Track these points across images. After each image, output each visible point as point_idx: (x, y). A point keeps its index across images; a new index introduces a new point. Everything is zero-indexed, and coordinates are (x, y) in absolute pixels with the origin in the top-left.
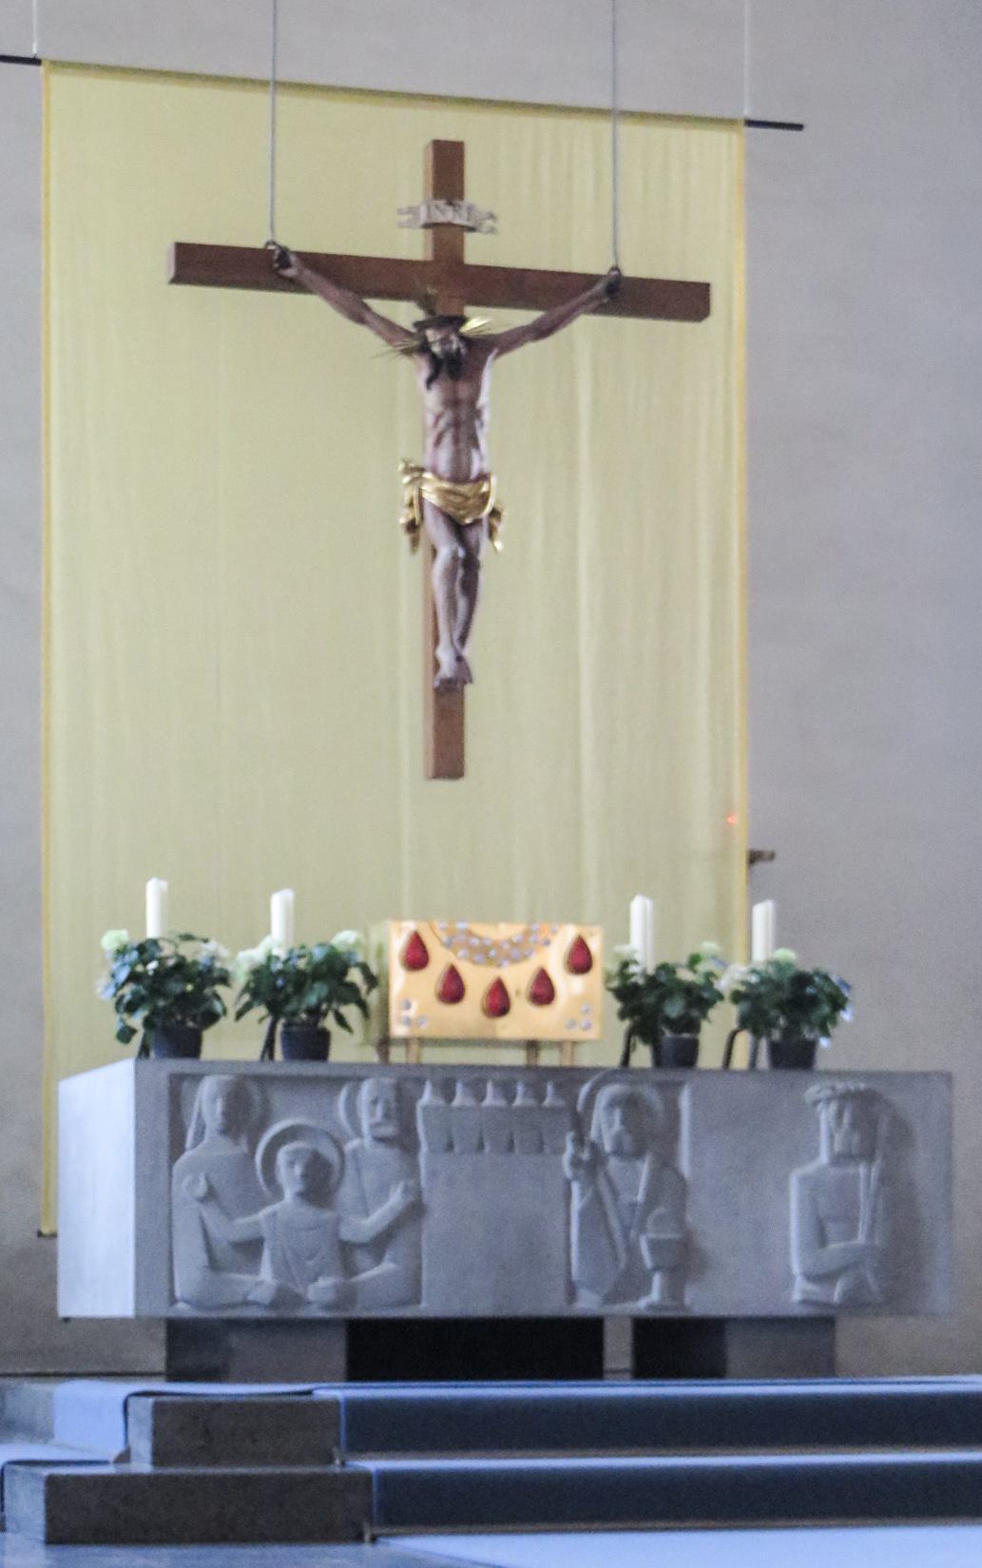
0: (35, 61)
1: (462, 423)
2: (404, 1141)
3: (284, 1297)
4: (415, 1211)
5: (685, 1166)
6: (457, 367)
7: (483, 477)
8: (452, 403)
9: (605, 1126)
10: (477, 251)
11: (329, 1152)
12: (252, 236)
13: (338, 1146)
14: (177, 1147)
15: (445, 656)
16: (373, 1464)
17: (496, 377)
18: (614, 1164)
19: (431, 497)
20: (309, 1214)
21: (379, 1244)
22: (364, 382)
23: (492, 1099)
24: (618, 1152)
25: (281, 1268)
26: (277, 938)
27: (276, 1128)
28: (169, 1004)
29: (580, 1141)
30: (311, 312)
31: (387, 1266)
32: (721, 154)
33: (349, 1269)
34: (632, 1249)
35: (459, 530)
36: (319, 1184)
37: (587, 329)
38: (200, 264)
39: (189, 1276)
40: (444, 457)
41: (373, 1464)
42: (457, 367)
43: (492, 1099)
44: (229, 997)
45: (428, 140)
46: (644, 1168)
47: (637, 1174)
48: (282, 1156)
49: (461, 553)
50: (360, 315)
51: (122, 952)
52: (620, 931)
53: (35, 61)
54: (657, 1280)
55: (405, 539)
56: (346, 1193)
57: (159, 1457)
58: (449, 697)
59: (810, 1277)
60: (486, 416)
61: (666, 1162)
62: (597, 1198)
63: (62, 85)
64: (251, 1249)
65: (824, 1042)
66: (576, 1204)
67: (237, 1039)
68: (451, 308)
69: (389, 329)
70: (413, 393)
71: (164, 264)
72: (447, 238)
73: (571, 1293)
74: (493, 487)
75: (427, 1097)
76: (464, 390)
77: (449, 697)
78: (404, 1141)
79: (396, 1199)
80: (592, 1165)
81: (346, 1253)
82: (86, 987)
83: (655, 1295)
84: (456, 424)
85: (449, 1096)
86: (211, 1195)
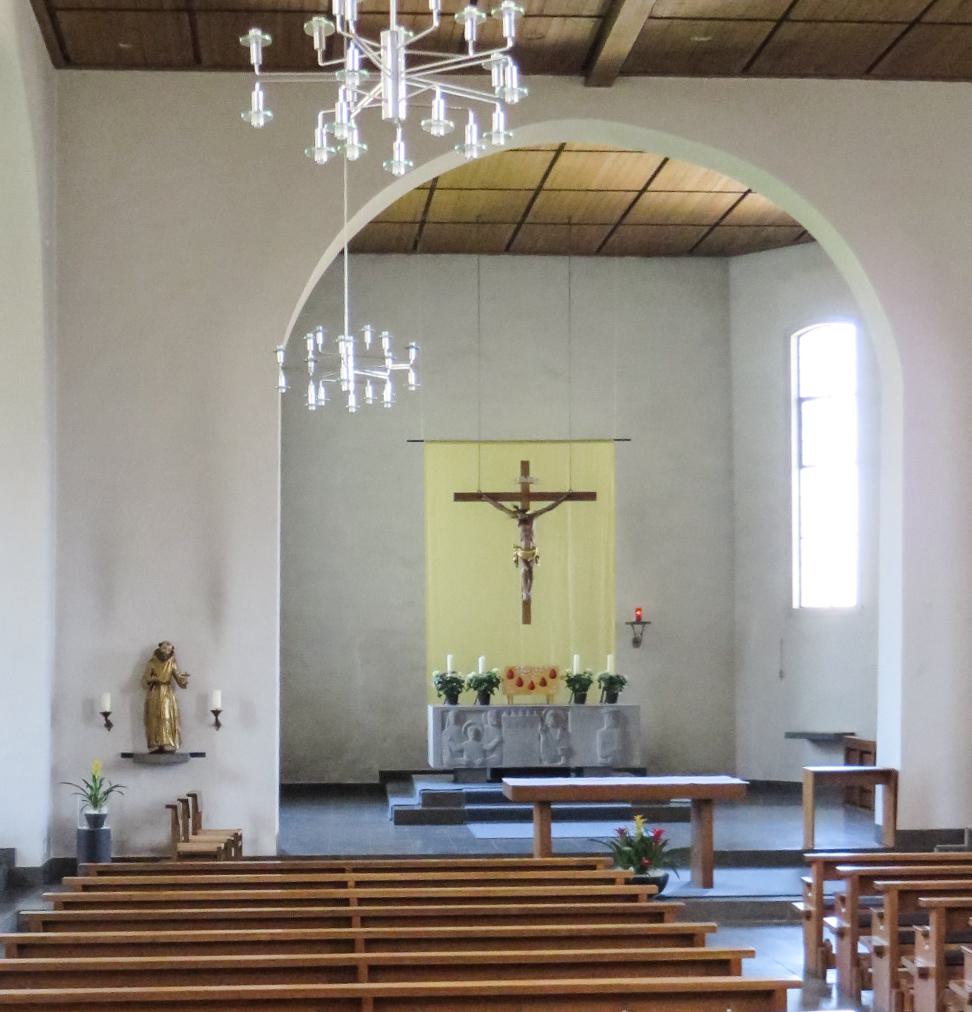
0: (422, 441)
1: (528, 535)
2: (499, 725)
3: (469, 763)
4: (501, 742)
5: (570, 730)
6: (526, 521)
7: (534, 548)
8: (525, 530)
9: (549, 720)
10: (533, 489)
11: (480, 728)
12: (474, 491)
13: (482, 726)
14: (443, 727)
15: (525, 595)
16: (467, 807)
17: (536, 523)
18: (551, 730)
19: (520, 554)
20: (475, 743)
21: (493, 750)
22: (502, 526)
23: (513, 715)
24: (553, 726)
25: (468, 757)
26: (481, 670)
27: (467, 723)
28: (451, 688)
29: (542, 725)
30: (486, 506)
31: (494, 755)
32: (608, 449)
33: (485, 756)
34: (556, 751)
35: (527, 563)
36: (478, 736)
37: (568, 505)
38: (459, 497)
39: (446, 758)
40: (523, 544)
41: (467, 807)
42: (526, 521)
43: (520, 714)
44: (465, 685)
45: (188, 690)
46: (559, 731)
47: (556, 733)
48: (469, 729)
49: (527, 569)
50: (502, 508)
51: (437, 676)
52: (569, 663)
53: (422, 441)
54: (563, 758)
55: (515, 565)
56: (485, 738)
57: (424, 805)
58: (527, 604)
59: (603, 757)
60: (535, 533)
61: (565, 729)
62: (547, 739)
63: (429, 445)
64: (461, 752)
65: (620, 693)
66: (542, 739)
67: (468, 698)
68: (525, 505)
69: (509, 511)
70: (514, 527)
71: (452, 497)
72: (525, 486)
73: (541, 761)
74: (537, 551)
75: (504, 715)
76: (528, 527)
77: (527, 604)
78: (499, 725)
79: (496, 740)
80: (546, 730)
81: (484, 753)
82: (433, 684)
83: (562, 761)
84: (526, 536)
85: (509, 714)
86: (451, 740)
